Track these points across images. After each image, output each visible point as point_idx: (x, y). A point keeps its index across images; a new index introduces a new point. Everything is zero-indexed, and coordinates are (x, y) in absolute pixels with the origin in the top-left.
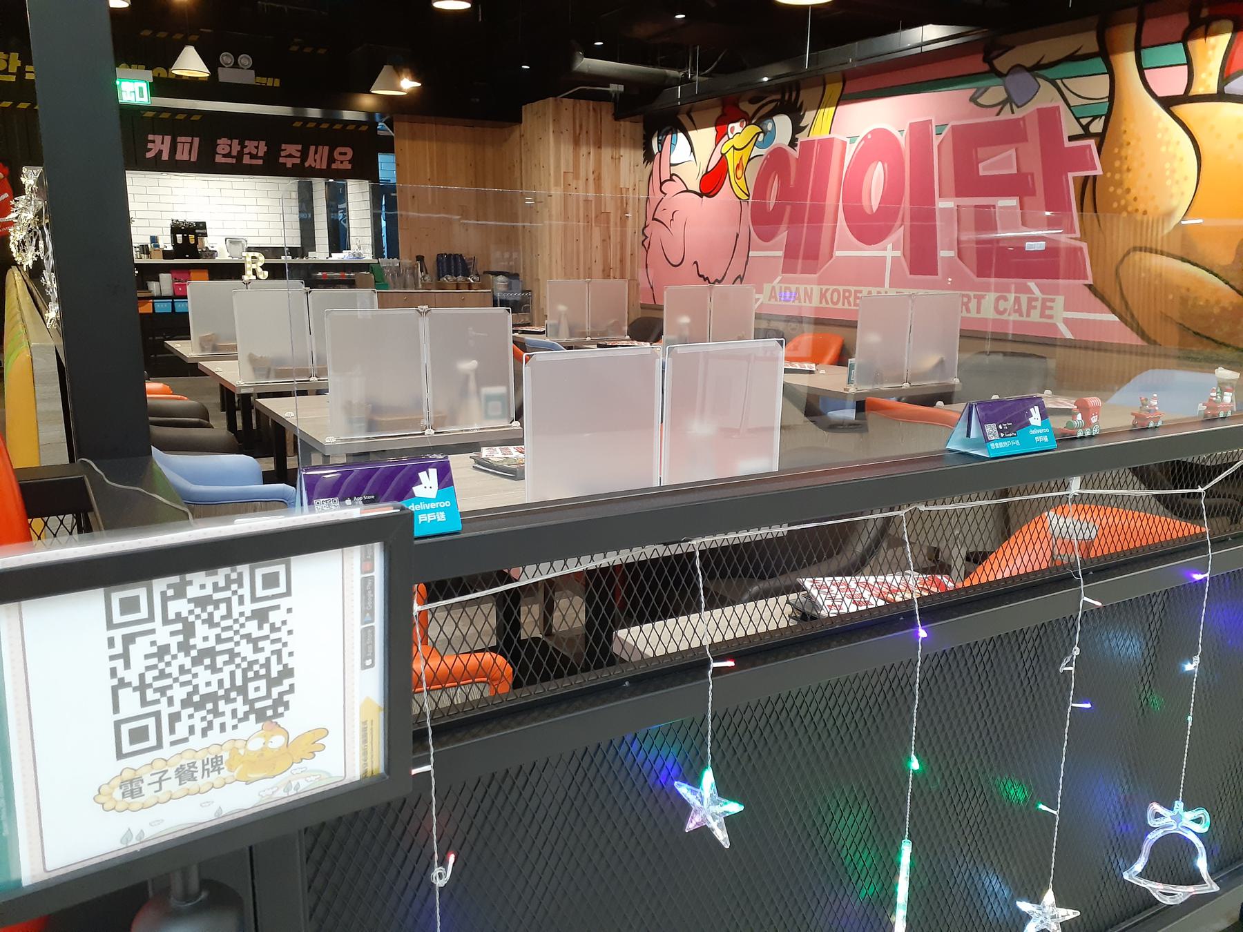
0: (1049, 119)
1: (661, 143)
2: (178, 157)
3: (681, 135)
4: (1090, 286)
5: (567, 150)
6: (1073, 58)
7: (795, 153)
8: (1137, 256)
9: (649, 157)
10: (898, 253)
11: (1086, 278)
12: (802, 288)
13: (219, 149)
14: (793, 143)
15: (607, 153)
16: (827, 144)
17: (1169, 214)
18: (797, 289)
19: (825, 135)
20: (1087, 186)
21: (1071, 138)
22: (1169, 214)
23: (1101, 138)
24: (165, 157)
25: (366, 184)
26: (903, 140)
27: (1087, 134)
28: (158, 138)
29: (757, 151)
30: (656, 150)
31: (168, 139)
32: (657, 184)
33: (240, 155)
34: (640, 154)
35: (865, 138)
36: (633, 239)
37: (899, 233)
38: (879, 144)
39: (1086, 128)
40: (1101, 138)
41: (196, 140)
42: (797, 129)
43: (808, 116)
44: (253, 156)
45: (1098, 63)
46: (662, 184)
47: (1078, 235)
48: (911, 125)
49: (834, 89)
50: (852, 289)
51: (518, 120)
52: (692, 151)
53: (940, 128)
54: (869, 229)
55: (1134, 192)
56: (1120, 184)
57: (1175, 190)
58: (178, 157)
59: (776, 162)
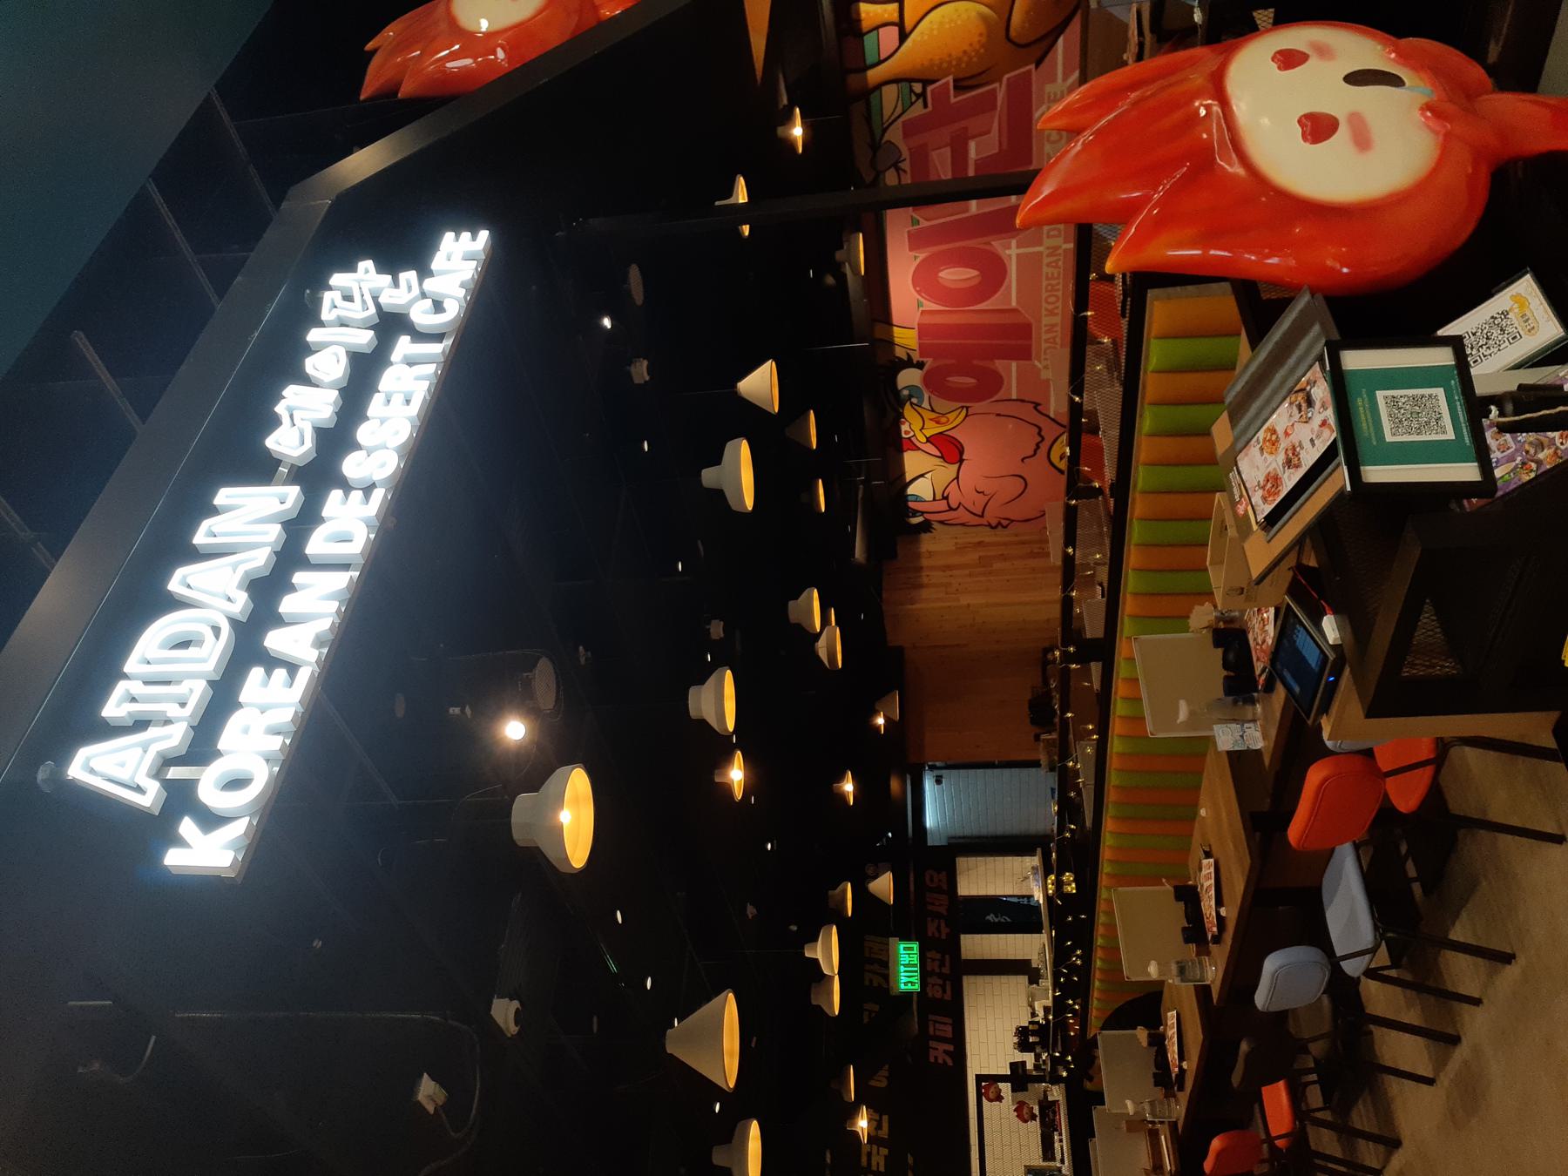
0: (910, 129)
1: (915, 513)
2: (950, 1035)
3: (910, 491)
4: (1037, 67)
5: (925, 593)
6: (868, 119)
7: (929, 362)
8: (1013, 33)
9: (926, 527)
10: (1014, 242)
11: (1029, 72)
12: (1044, 337)
13: (938, 995)
14: (920, 366)
15: (925, 562)
16: (923, 331)
17: (984, 18)
18: (1047, 341)
19: (914, 334)
20: (961, 86)
21: (925, 106)
22: (984, 18)
23: (926, 82)
24: (951, 1048)
25: (962, 863)
26: (921, 256)
27: (923, 95)
28: (932, 1053)
29: (926, 404)
30: (920, 519)
31: (933, 1044)
32: (951, 514)
33: (940, 975)
34: (925, 536)
35: (919, 292)
36: (1001, 536)
37: (997, 245)
38: (924, 280)
39: (918, 96)
40: (926, 82)
41: (931, 1017)
42: (909, 363)
43: (900, 353)
44: (942, 964)
45: (874, 98)
46: (951, 509)
47: (996, 85)
48: (911, 249)
49: (879, 331)
50: (1044, 283)
51: (900, 650)
52: (922, 476)
53: (915, 222)
54: (993, 274)
55: (966, 47)
56: (959, 60)
57: (964, 16)
58: (950, 1035)
59: (936, 383)
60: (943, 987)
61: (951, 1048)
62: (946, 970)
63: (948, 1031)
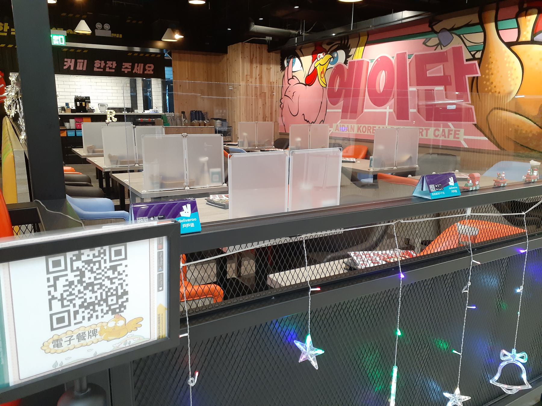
0: (457, 52)
1: (288, 62)
2: (78, 68)
3: (297, 59)
4: (475, 125)
5: (247, 65)
6: (468, 25)
7: (346, 67)
8: (496, 111)
9: (283, 68)
10: (392, 110)
11: (473, 121)
12: (350, 125)
13: (95, 65)
14: (346, 62)
15: (265, 67)
16: (361, 63)
17: (510, 93)
18: (348, 126)
19: (360, 59)
20: (474, 81)
21: (467, 60)
22: (510, 93)
23: (480, 60)
24: (72, 68)
25: (160, 80)
26: (394, 61)
27: (474, 58)
28: (69, 60)
29: (330, 66)
30: (286, 65)
31: (73, 60)
32: (287, 80)
33: (105, 67)
34: (279, 67)
35: (377, 60)
36: (276, 104)
37: (392, 101)
38: (383, 63)
39: (473, 56)
40: (480, 60)
41: (86, 61)
42: (347, 56)
43: (352, 51)
44: (110, 68)
45: (479, 28)
46: (289, 80)
47: (470, 102)
48: (397, 55)
49: (364, 39)
50: (372, 126)
51: (226, 52)
52: (302, 66)
53: (410, 56)
54: (379, 100)
55: (494, 84)
56: (488, 80)
57: (512, 83)
58: (78, 68)
59: (338, 71)
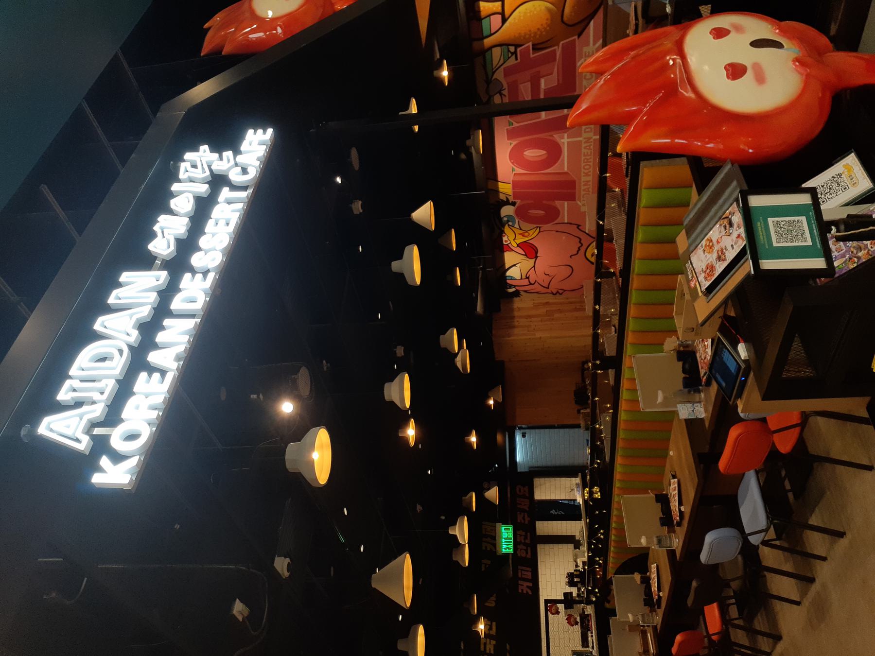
0: (508, 72)
1: (511, 286)
2: (530, 577)
3: (508, 274)
4: (579, 37)
5: (516, 331)
6: (485, 67)
7: (518, 202)
8: (565, 19)
9: (517, 294)
10: (566, 135)
11: (574, 40)
12: (583, 188)
13: (524, 555)
14: (513, 204)
15: (516, 314)
16: (515, 184)
17: (549, 10)
18: (584, 190)
19: (510, 186)
20: (536, 48)
21: (516, 59)
22: (549, 10)
23: (517, 46)
24: (531, 585)
25: (537, 481)
26: (514, 143)
27: (515, 53)
28: (520, 588)
29: (517, 226)
30: (514, 290)
31: (520, 582)
32: (531, 287)
33: (525, 544)
34: (516, 299)
35: (513, 163)
36: (558, 299)
37: (556, 137)
38: (516, 156)
39: (512, 54)
40: (517, 46)
41: (519, 567)
42: (507, 203)
43: (502, 197)
44: (526, 538)
45: (488, 55)
46: (531, 284)
47: (556, 47)
48: (508, 139)
49: (490, 185)
50: (583, 158)
51: (502, 362)
52: (515, 265)
53: (510, 124)
54: (554, 153)
55: (539, 26)
56: (535, 33)
57: (538, 9)
58: (530, 577)
59: (522, 214)
60: (526, 551)
61: (531, 585)
62: (528, 541)
63: (529, 575)
